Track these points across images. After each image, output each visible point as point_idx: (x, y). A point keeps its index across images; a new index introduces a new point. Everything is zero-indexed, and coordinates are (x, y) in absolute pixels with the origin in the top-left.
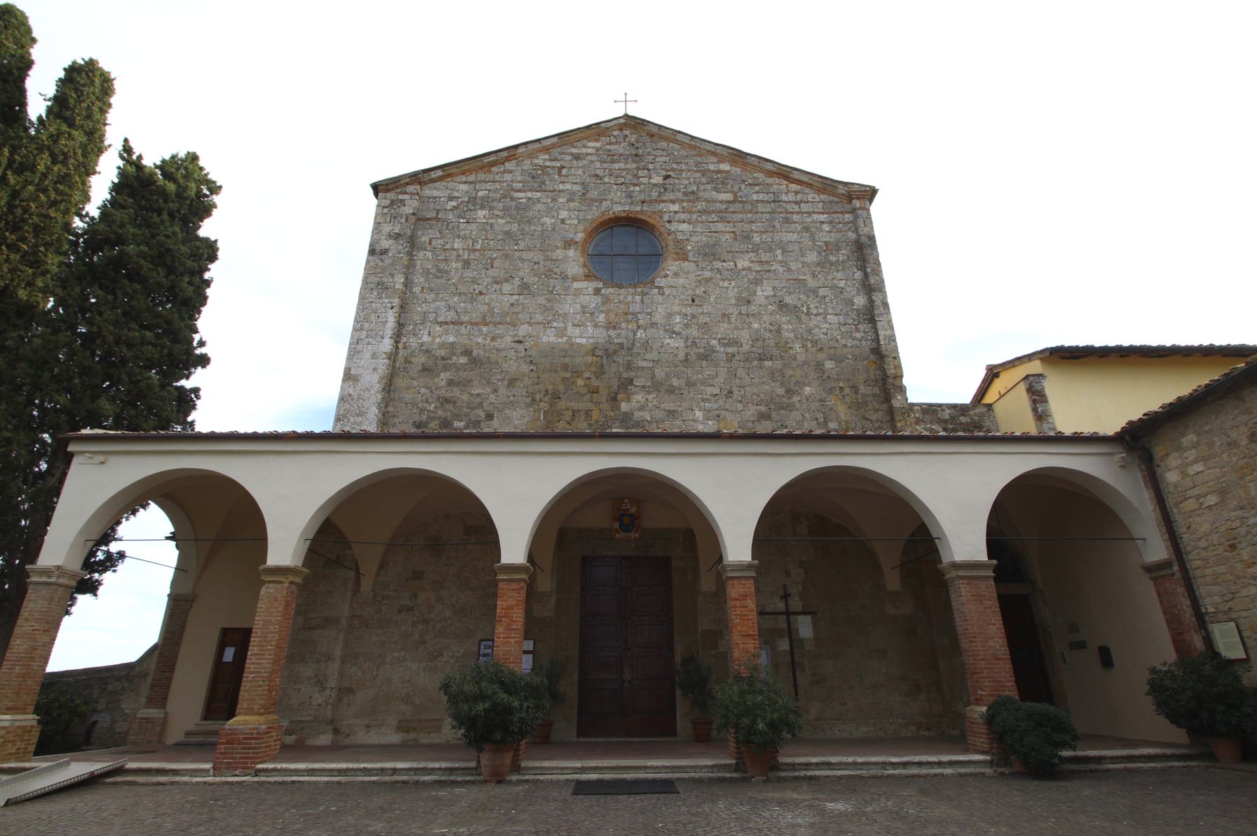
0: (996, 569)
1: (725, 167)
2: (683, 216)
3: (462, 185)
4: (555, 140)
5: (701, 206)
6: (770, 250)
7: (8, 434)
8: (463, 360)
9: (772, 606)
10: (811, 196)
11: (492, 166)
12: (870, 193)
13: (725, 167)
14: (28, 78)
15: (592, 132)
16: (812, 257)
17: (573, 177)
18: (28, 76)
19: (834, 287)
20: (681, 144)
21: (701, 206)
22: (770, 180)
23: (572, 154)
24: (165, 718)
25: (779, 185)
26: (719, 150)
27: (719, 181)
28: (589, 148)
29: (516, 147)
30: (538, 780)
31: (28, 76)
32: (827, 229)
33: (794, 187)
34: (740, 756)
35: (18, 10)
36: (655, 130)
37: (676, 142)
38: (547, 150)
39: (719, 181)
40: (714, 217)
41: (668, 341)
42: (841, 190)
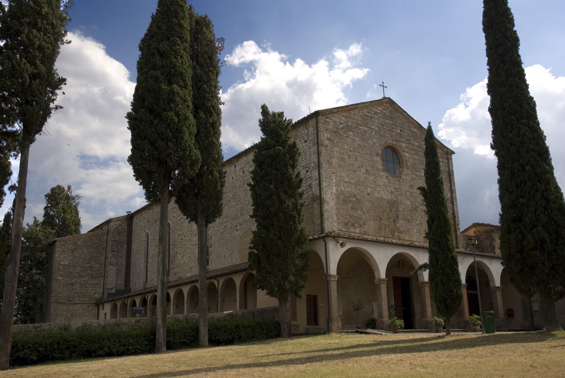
0: (467, 286)
3: (343, 117)
4: (369, 103)
8: (354, 199)
11: (351, 110)
12: (454, 153)
14: (483, 6)
15: (379, 102)
17: (24, 94)
18: (483, 7)
20: (404, 116)
23: (374, 112)
24: (132, 307)
26: (415, 123)
28: (378, 109)
29: (359, 104)
31: (483, 7)
36: (397, 107)
37: (403, 114)
38: (366, 107)
41: (406, 202)
42: (445, 150)
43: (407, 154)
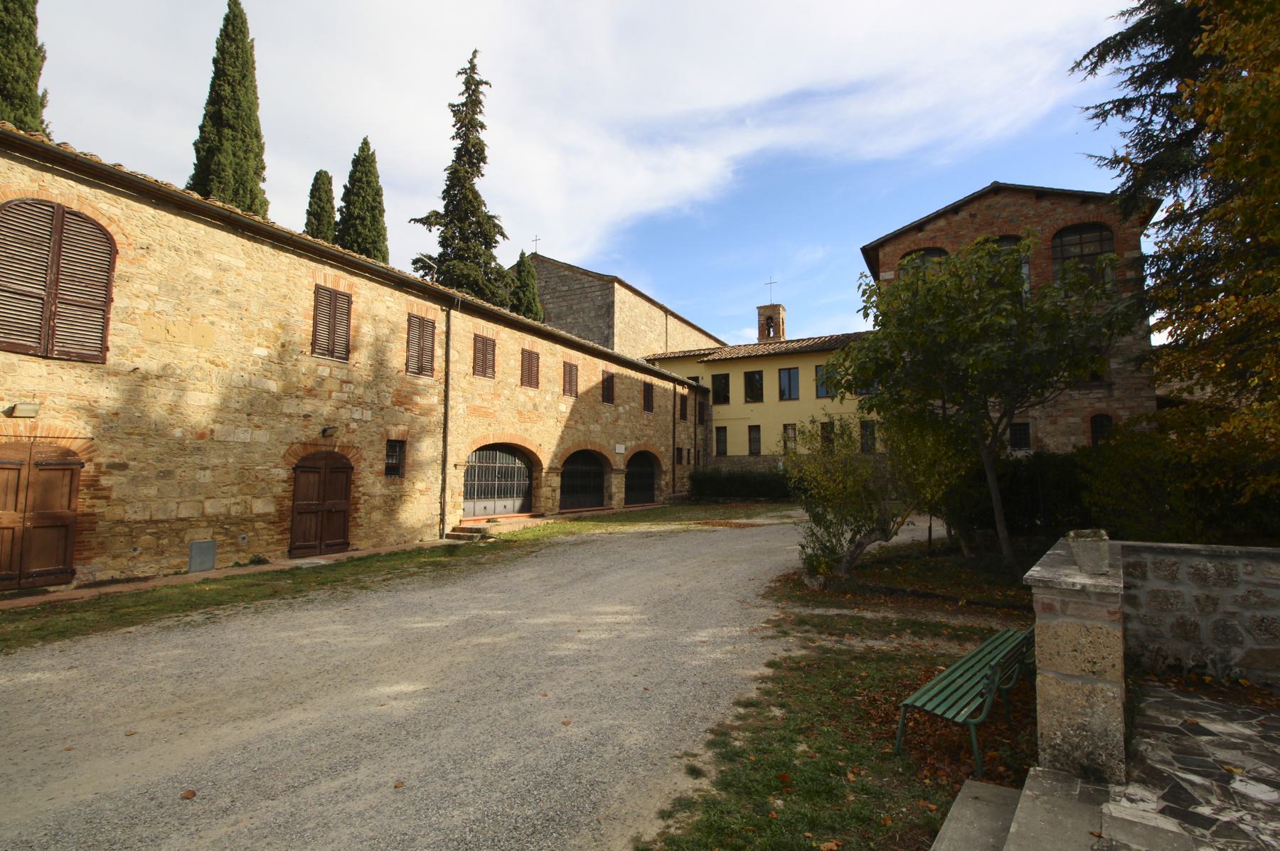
1: (567, 273)
2: (550, 301)
5: (557, 294)
6: (578, 312)
7: (32, 677)
9: (1118, 735)
10: (597, 283)
13: (567, 273)
16: (593, 314)
19: (599, 327)
21: (557, 294)
22: (582, 277)
25: (585, 279)
27: (563, 280)
30: (298, 568)
32: (265, 322)
33: (590, 279)
34: (718, 738)
35: (253, 76)
39: (563, 280)
40: (561, 300)
43: (551, 306)
